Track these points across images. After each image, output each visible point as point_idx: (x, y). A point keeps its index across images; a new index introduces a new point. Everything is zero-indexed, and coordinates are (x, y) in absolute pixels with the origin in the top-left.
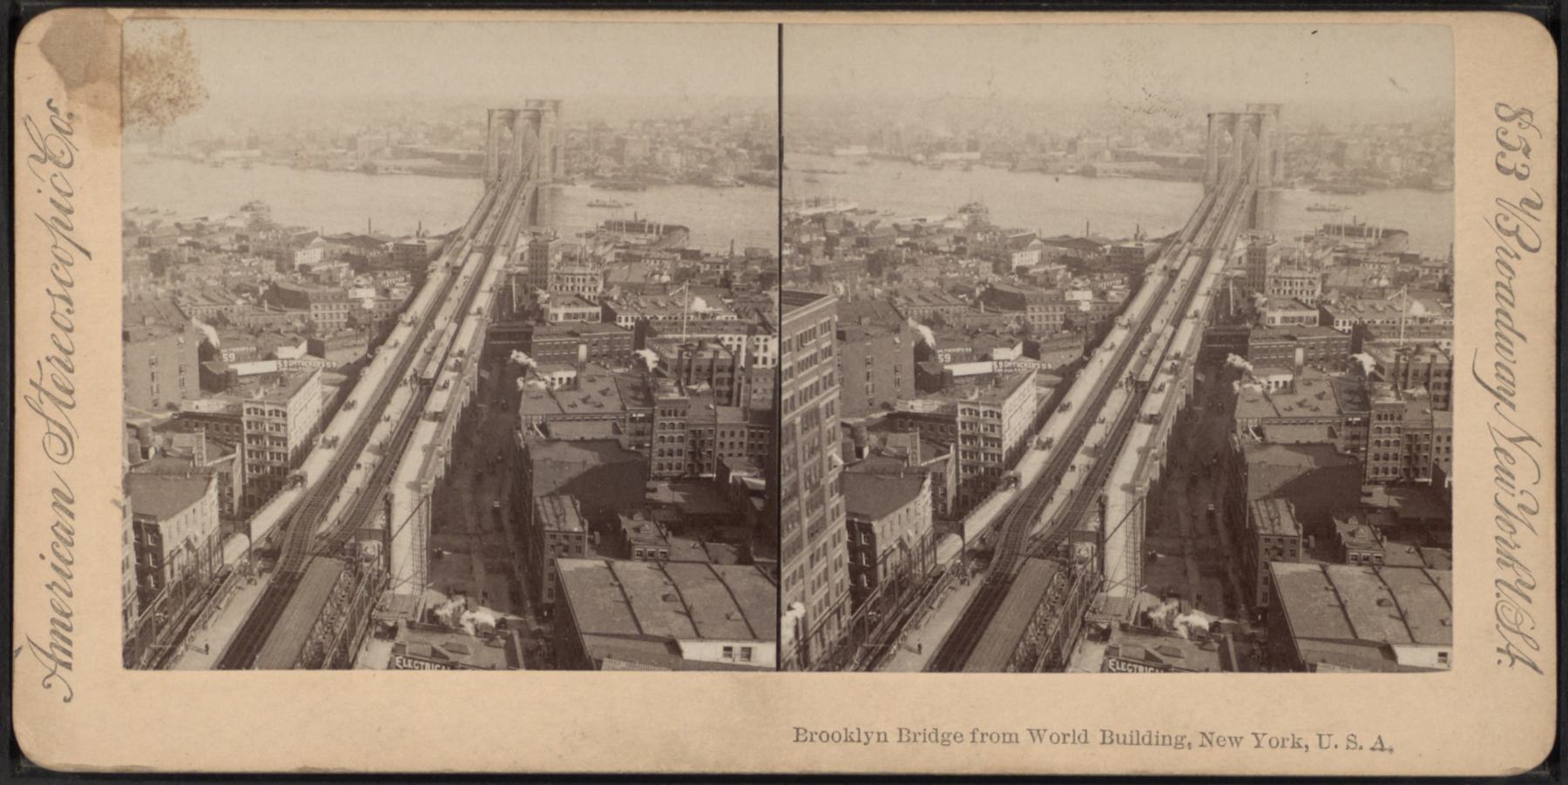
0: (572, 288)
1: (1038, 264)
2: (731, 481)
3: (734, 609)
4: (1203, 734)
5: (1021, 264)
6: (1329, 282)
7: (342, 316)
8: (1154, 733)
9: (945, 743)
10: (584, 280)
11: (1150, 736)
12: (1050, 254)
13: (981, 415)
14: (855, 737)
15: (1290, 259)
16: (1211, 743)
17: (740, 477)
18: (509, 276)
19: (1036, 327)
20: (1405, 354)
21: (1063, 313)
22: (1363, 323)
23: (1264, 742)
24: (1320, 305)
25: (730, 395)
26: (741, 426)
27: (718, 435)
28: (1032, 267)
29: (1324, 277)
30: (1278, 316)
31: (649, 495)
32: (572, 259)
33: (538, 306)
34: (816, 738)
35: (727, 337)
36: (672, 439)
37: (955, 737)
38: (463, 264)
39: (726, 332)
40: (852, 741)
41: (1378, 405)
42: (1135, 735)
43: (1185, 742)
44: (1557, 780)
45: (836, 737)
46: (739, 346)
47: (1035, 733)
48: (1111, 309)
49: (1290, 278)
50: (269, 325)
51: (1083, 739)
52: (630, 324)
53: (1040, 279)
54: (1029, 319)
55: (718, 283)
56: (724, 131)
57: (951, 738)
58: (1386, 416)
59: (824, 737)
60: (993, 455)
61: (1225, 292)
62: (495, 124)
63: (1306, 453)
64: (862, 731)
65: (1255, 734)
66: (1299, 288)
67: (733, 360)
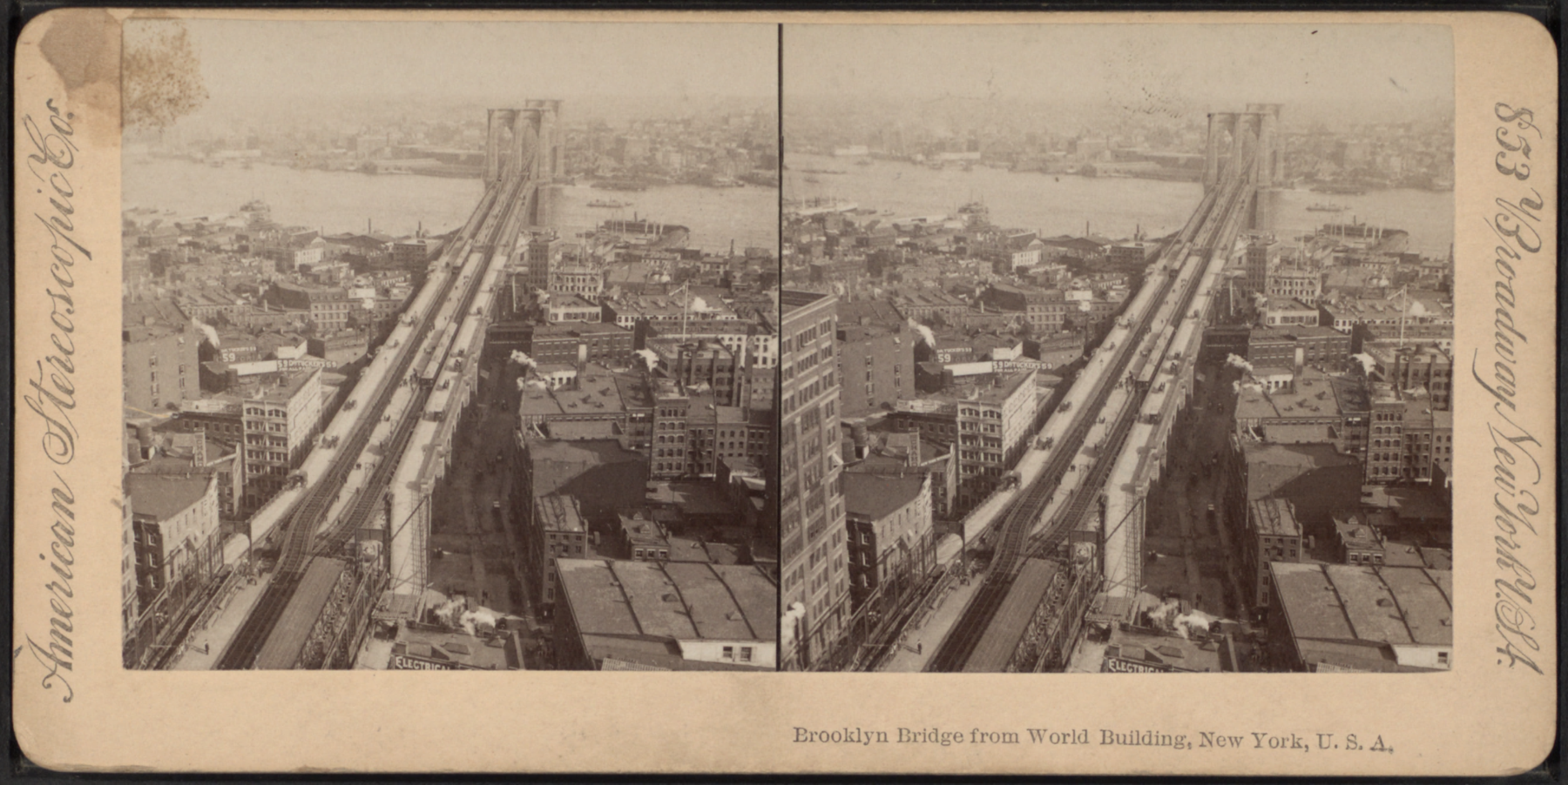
1: (1038, 264)
2: (731, 481)
3: (734, 608)
4: (1203, 734)
6: (1329, 282)
8: (1154, 733)
9: (945, 743)
10: (1302, 284)
11: (1150, 736)
13: (981, 415)
14: (855, 737)
16: (1210, 743)
17: (740, 477)
18: (509, 276)
19: (320, 326)
21: (1062, 313)
23: (1264, 742)
24: (1320, 305)
28: (315, 265)
29: (1324, 277)
31: (649, 495)
34: (816, 738)
37: (955, 737)
39: (726, 332)
40: (852, 740)
41: (1378, 406)
42: (1135, 735)
43: (1185, 742)
44: (1557, 780)
45: (836, 737)
46: (739, 346)
47: (1035, 733)
50: (269, 325)
51: (1083, 739)
53: (1040, 279)
55: (718, 282)
56: (724, 131)
57: (951, 738)
59: (824, 737)
60: (993, 455)
61: (1225, 292)
64: (862, 731)
65: (1255, 734)
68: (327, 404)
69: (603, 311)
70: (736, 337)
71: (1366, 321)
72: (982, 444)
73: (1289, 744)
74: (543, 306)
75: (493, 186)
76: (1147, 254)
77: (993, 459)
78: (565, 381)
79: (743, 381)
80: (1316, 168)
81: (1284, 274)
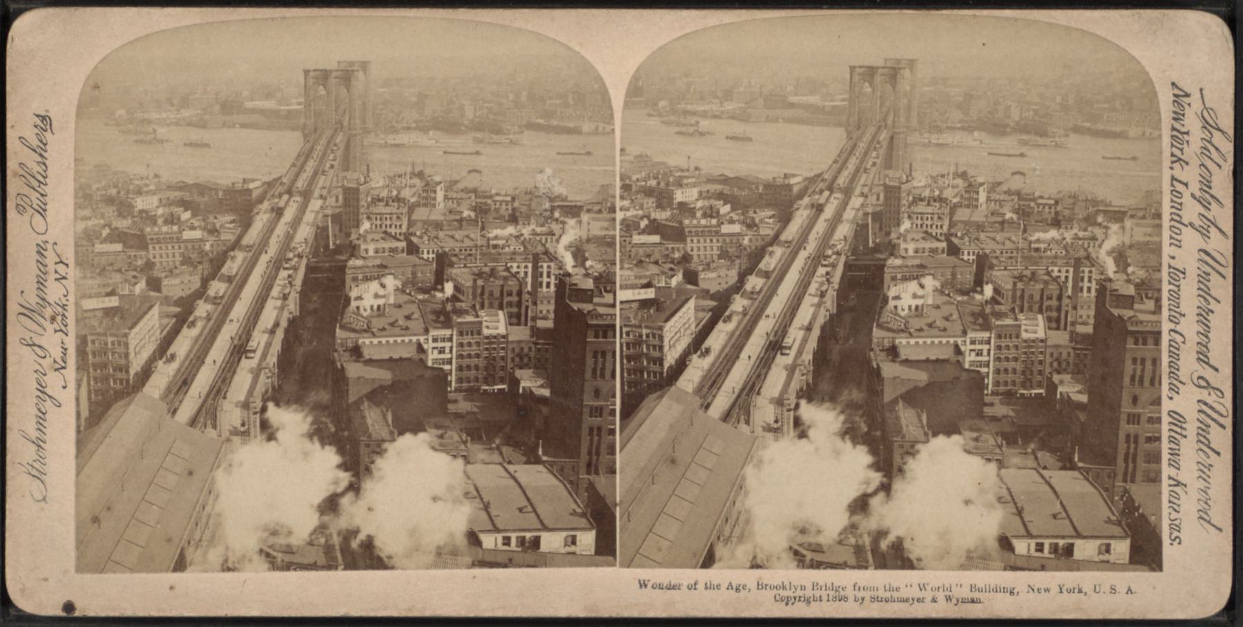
0: (921, 226)
2: (521, 391)
3: (526, 503)
7: (715, 248)
10: (932, 218)
12: (708, 191)
13: (644, 337)
15: (381, 197)
18: (326, 216)
19: (695, 257)
20: (481, 278)
22: (445, 252)
24: (407, 237)
25: (1058, 320)
27: (1048, 356)
30: (911, 247)
33: (351, 242)
35: (1056, 269)
36: (1007, 359)
46: (1067, 277)
48: (225, 245)
50: (649, 256)
54: (151, 256)
55: (507, 218)
58: (1010, 338)
60: (655, 373)
61: (864, 227)
62: (856, 78)
68: (700, 327)
69: (408, 245)
72: (645, 363)
74: (356, 242)
78: (375, 308)
79: (530, 304)
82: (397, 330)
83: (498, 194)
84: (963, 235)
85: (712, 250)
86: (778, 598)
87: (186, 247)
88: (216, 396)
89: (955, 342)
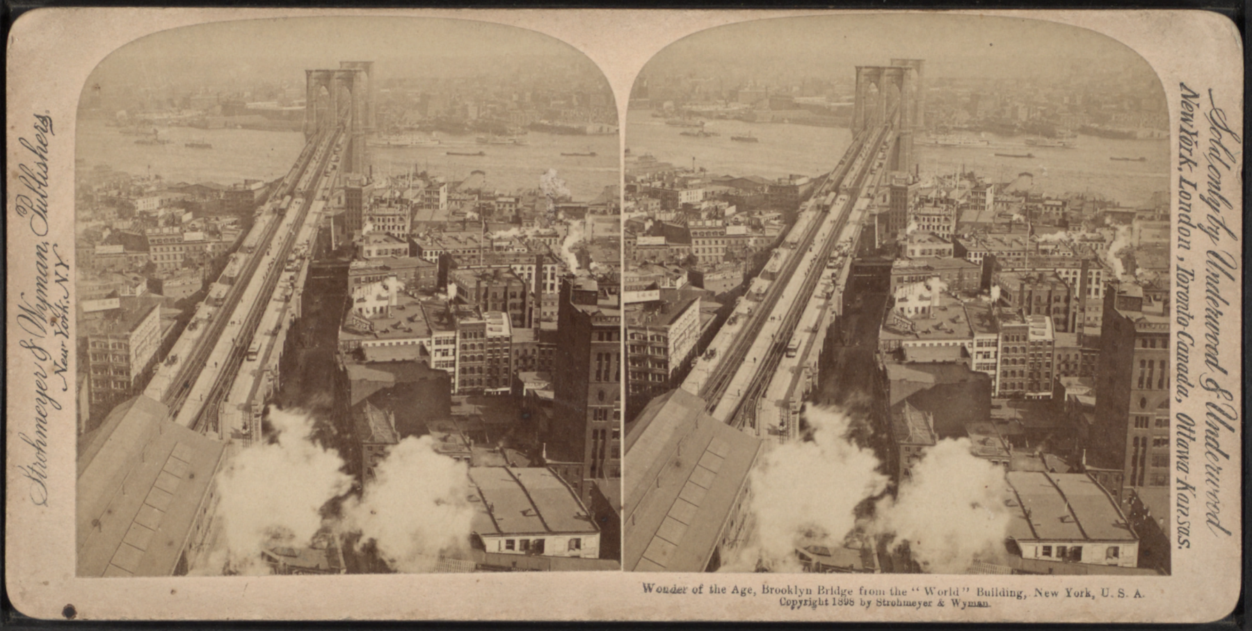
0: (928, 227)
2: (525, 394)
3: (529, 506)
5: (689, 201)
7: (720, 250)
10: (939, 220)
12: (713, 193)
14: (793, 591)
17: (1075, 396)
18: (872, 216)
19: (700, 259)
21: (725, 246)
22: (448, 253)
23: (1072, 594)
24: (410, 238)
26: (533, 344)
31: (994, 412)
32: (383, 201)
36: (1014, 362)
38: (287, 208)
41: (463, 325)
46: (1074, 279)
49: (928, 215)
50: (653, 258)
52: (979, 259)
55: (1057, 223)
60: (660, 375)
61: (871, 228)
63: (385, 370)
66: (936, 224)
67: (524, 287)
69: (955, 248)
70: (527, 267)
71: (995, 253)
72: (650, 365)
73: (1084, 594)
74: (358, 244)
75: (313, 135)
76: (257, 195)
77: (660, 379)
80: (953, 117)
81: (377, 211)
82: (400, 333)
83: (1049, 199)
84: (970, 236)
85: (717, 251)
86: (783, 602)
87: (730, 242)
88: (753, 398)
89: (421, 342)
